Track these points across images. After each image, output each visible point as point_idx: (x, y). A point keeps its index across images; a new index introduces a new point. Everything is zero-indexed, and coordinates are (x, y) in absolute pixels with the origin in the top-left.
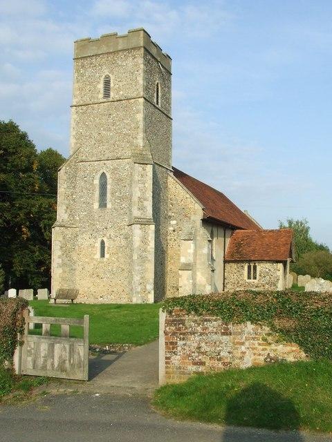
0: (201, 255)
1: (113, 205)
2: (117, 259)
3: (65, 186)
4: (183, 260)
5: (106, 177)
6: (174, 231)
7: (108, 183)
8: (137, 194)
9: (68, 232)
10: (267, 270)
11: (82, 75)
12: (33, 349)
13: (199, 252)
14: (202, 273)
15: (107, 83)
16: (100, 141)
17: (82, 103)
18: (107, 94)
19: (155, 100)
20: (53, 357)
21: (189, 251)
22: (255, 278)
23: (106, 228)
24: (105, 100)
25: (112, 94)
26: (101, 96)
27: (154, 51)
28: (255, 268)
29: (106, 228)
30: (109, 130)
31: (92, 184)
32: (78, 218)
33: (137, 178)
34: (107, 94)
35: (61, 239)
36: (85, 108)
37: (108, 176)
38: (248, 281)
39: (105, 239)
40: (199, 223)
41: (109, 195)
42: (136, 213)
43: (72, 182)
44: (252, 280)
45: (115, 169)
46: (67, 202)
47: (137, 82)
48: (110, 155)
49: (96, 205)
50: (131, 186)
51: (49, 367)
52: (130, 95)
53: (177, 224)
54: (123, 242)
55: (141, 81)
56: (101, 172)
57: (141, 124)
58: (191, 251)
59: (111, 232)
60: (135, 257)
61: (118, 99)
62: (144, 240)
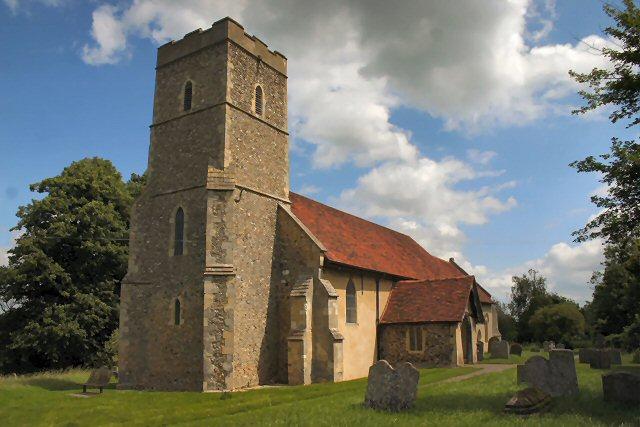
6: (287, 285)
15: (188, 91)
18: (188, 105)
19: (253, 108)
22: (420, 348)
25: (193, 105)
26: (181, 108)
28: (419, 334)
30: (189, 151)
34: (188, 105)
38: (410, 352)
43: (146, 223)
46: (137, 250)
49: (171, 253)
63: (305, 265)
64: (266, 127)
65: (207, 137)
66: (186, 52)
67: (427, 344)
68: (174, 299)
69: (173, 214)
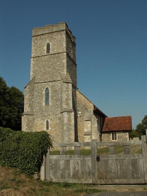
0: (94, 128)
1: (52, 103)
2: (55, 130)
3: (29, 95)
4: (86, 130)
5: (48, 90)
7: (50, 93)
8: (65, 97)
9: (30, 117)
10: (121, 135)
11: (36, 43)
12: (54, 165)
13: (93, 126)
14: (95, 136)
15: (48, 46)
16: (45, 73)
17: (36, 56)
20: (69, 169)
21: (88, 126)
22: (116, 139)
23: (49, 115)
24: (47, 54)
25: (51, 51)
26: (45, 52)
27: (69, 33)
29: (49, 115)
31: (42, 94)
32: (35, 111)
33: (64, 89)
35: (27, 121)
36: (37, 58)
37: (50, 89)
39: (49, 120)
40: (92, 112)
41: (50, 99)
42: (65, 106)
44: (114, 140)
45: (53, 86)
46: (29, 103)
47: (63, 45)
48: (50, 80)
49: (44, 104)
50: (61, 93)
51: (66, 175)
52: (60, 52)
53: (82, 113)
54: (58, 122)
55: (65, 45)
56: (46, 87)
57: (65, 65)
58: (90, 126)
59: (52, 117)
60: (65, 128)
61: (54, 53)
62: (69, 120)
63: (88, 110)
64: (54, 55)
65: (58, 64)
66: (47, 32)
67: (118, 138)
68: (46, 120)
69: (44, 90)
